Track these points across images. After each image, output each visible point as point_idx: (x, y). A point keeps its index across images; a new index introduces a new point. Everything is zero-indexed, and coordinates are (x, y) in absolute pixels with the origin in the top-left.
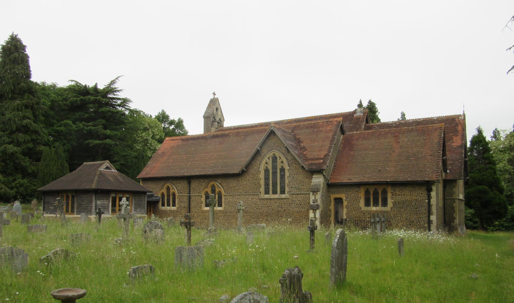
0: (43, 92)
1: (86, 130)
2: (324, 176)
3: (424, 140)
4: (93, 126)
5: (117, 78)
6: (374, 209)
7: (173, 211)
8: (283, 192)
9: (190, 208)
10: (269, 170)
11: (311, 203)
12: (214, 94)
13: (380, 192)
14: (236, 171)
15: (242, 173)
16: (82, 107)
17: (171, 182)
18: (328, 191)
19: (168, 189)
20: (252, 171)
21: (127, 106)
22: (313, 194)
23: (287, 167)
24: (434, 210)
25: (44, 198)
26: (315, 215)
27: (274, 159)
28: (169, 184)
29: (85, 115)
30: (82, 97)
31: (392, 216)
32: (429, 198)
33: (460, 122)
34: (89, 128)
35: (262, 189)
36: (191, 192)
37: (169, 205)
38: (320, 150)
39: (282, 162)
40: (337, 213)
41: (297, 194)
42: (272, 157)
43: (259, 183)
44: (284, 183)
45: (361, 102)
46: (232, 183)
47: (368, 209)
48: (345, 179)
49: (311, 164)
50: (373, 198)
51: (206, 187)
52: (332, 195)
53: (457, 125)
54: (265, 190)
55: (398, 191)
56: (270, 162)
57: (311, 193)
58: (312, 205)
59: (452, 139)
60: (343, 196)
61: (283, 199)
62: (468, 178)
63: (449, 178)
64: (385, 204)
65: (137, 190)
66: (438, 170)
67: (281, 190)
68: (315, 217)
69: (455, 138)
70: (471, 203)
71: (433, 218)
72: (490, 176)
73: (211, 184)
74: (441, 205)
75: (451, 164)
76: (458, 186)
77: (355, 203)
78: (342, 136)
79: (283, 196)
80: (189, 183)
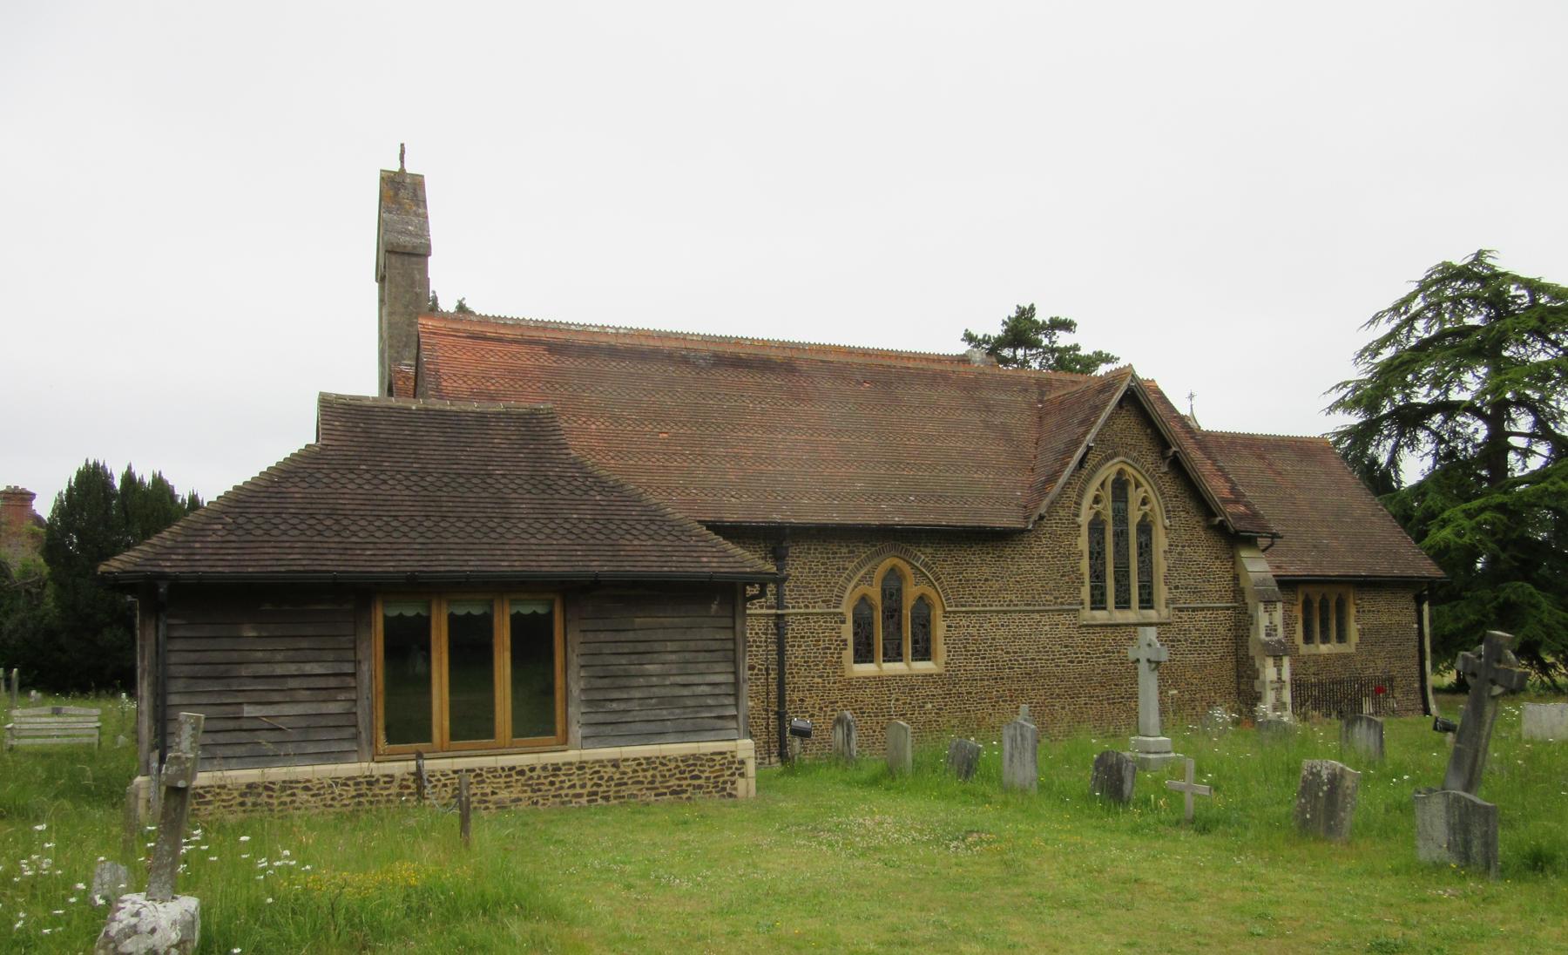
6: (1324, 649)
8: (1147, 602)
10: (1103, 522)
23: (1160, 523)
27: (1120, 487)
36: (788, 600)
41: (1194, 610)
43: (1075, 569)
46: (979, 565)
57: (1261, 606)
64: (1342, 638)
73: (889, 562)
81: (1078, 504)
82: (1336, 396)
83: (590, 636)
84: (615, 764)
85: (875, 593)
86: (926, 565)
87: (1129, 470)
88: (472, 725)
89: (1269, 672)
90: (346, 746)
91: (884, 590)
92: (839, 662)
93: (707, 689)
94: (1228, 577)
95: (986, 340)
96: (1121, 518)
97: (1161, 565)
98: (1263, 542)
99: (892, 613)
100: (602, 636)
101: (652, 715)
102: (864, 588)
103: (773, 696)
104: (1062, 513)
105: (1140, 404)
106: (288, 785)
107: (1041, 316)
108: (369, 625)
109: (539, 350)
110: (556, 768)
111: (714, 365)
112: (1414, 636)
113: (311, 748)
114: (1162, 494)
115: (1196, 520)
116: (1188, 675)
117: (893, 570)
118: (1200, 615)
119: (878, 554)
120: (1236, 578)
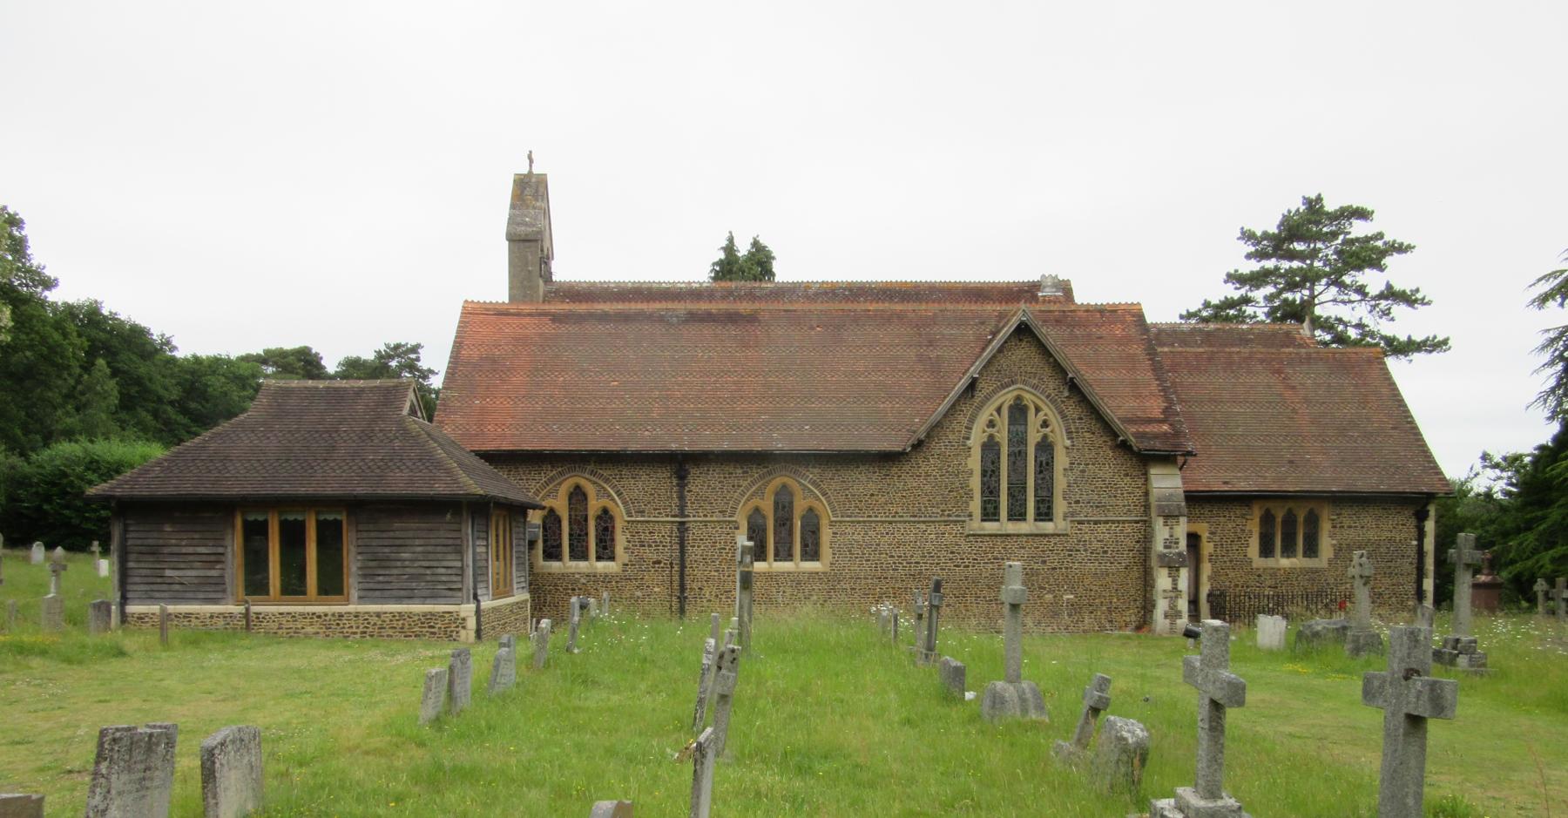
6: (1285, 562)
7: (606, 579)
8: (1045, 514)
9: (683, 566)
10: (998, 444)
17: (592, 473)
19: (578, 496)
20: (937, 447)
22: (1166, 524)
23: (1061, 441)
25: (126, 531)
26: (1175, 582)
27: (1018, 412)
35: (976, 506)
37: (579, 553)
39: (1045, 424)
41: (1096, 523)
44: (1050, 490)
45: (731, 240)
46: (863, 481)
51: (760, 493)
54: (984, 509)
55: (1347, 516)
56: (1003, 422)
61: (1046, 535)
64: (1311, 549)
65: (302, 491)
67: (1037, 508)
68: (1175, 589)
73: (778, 482)
79: (1048, 527)
81: (969, 428)
82: (1545, 287)
83: (365, 535)
84: (378, 615)
85: (767, 506)
86: (814, 483)
87: (1027, 396)
88: (293, 587)
89: (1163, 581)
90: (220, 595)
91: (776, 504)
93: (443, 571)
94: (1139, 492)
95: (1266, 236)
96: (1018, 440)
97: (1060, 482)
98: (1180, 460)
99: (784, 522)
100: (373, 534)
101: (405, 585)
102: (756, 502)
103: (676, 585)
105: (1029, 331)
106: (187, 616)
107: (1330, 206)
108: (233, 526)
109: (546, 320)
110: (341, 615)
111: (686, 321)
112: (1413, 553)
113: (201, 596)
114: (1064, 417)
115: (1100, 440)
116: (1086, 582)
117: (784, 486)
118: (1103, 527)
119: (770, 473)
120: (1147, 494)
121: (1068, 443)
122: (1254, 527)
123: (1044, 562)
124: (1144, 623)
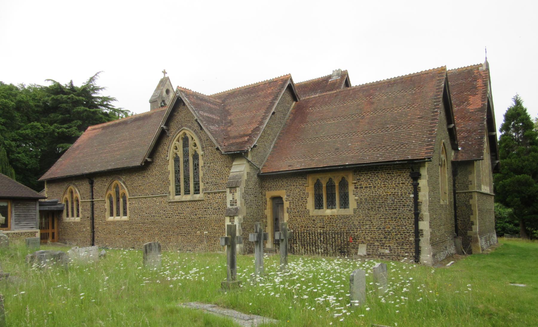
0: (9, 92)
1: (58, 133)
2: (249, 162)
3: (413, 94)
4: (67, 128)
5: (96, 75)
8: (197, 191)
10: (178, 158)
11: (229, 206)
12: (165, 72)
13: (337, 184)
14: (138, 163)
15: (145, 167)
16: (55, 108)
17: (74, 184)
18: (262, 187)
20: (158, 161)
21: (111, 105)
23: (200, 152)
24: (425, 211)
27: (185, 140)
28: (72, 187)
29: (58, 116)
30: (53, 96)
31: (356, 223)
32: (416, 190)
33: (480, 75)
34: (60, 130)
35: (172, 188)
36: (94, 197)
38: (250, 123)
39: (195, 145)
40: (276, 220)
41: (215, 193)
42: (183, 139)
43: (167, 178)
46: (137, 180)
47: (320, 212)
48: (284, 165)
49: (232, 145)
50: (327, 194)
52: (267, 192)
53: (475, 79)
55: (365, 180)
56: (180, 145)
57: (228, 190)
58: (229, 210)
59: (467, 100)
60: (282, 193)
62: (497, 161)
63: (460, 158)
64: (345, 204)
66: (431, 141)
69: (472, 99)
70: (508, 200)
71: (424, 225)
72: (533, 161)
74: (446, 200)
75: (466, 137)
76: (479, 171)
77: (301, 205)
78: (294, 103)
79: (197, 197)
80: (92, 183)
85: (112, 192)
92: (104, 217)
104: (163, 156)
118: (218, 195)
121: (202, 153)
122: (310, 190)
123: (196, 215)
124: (417, 259)
